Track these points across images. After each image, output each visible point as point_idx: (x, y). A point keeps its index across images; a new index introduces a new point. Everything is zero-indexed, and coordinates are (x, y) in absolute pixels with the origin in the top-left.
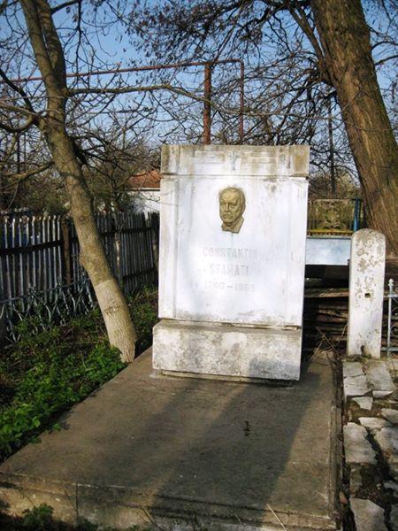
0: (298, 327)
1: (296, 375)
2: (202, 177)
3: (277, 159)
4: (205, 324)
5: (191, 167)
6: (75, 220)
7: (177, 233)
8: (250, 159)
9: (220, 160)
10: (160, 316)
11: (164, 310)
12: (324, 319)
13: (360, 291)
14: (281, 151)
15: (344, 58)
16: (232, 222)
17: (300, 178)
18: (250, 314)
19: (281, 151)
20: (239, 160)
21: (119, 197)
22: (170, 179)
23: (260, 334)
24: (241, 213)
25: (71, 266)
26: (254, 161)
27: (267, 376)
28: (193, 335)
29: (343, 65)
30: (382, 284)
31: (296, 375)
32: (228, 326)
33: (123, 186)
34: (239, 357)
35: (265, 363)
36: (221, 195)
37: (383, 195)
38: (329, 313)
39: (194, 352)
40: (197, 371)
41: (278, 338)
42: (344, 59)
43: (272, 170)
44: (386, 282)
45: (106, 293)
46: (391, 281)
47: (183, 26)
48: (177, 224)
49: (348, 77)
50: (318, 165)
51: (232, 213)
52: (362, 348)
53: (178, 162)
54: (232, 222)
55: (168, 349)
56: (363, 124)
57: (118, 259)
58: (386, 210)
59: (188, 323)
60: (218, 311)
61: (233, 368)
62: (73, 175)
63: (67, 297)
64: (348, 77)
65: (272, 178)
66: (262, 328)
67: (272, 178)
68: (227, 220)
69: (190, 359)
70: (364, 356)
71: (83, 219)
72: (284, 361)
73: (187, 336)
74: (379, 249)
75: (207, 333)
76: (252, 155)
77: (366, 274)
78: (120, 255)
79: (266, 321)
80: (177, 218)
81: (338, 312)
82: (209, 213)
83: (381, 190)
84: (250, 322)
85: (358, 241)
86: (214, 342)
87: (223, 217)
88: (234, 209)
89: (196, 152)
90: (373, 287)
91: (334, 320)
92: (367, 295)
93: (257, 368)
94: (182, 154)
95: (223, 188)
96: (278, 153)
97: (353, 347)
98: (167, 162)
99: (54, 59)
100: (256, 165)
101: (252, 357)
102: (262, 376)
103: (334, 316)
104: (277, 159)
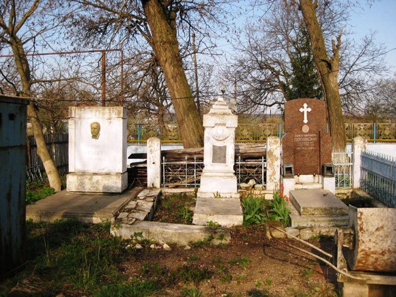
2: (84, 118)
3: (111, 112)
5: (80, 115)
6: (35, 135)
8: (102, 112)
10: (70, 171)
11: (71, 169)
15: (165, 56)
18: (103, 169)
20: (98, 112)
21: (56, 123)
23: (107, 176)
25: (31, 159)
27: (109, 192)
28: (82, 177)
29: (165, 59)
32: (95, 174)
33: (59, 116)
36: (91, 125)
38: (142, 172)
39: (82, 184)
40: (83, 191)
42: (165, 56)
44: (162, 158)
45: (48, 165)
46: (164, 157)
47: (93, 29)
49: (167, 65)
51: (96, 132)
52: (153, 184)
53: (75, 113)
55: (72, 183)
56: (175, 88)
57: (54, 156)
59: (81, 174)
60: (91, 169)
61: (97, 189)
62: (34, 117)
63: (29, 173)
64: (167, 65)
66: (108, 174)
67: (110, 119)
69: (80, 186)
70: (154, 187)
71: (38, 135)
72: (115, 185)
73: (79, 178)
74: (157, 145)
75: (87, 176)
78: (56, 155)
79: (109, 172)
82: (88, 132)
83: (185, 120)
86: (89, 179)
87: (92, 133)
88: (96, 130)
90: (155, 160)
92: (154, 163)
93: (105, 188)
94: (77, 111)
96: (112, 110)
98: (71, 113)
99: (25, 68)
102: (107, 191)
104: (111, 112)
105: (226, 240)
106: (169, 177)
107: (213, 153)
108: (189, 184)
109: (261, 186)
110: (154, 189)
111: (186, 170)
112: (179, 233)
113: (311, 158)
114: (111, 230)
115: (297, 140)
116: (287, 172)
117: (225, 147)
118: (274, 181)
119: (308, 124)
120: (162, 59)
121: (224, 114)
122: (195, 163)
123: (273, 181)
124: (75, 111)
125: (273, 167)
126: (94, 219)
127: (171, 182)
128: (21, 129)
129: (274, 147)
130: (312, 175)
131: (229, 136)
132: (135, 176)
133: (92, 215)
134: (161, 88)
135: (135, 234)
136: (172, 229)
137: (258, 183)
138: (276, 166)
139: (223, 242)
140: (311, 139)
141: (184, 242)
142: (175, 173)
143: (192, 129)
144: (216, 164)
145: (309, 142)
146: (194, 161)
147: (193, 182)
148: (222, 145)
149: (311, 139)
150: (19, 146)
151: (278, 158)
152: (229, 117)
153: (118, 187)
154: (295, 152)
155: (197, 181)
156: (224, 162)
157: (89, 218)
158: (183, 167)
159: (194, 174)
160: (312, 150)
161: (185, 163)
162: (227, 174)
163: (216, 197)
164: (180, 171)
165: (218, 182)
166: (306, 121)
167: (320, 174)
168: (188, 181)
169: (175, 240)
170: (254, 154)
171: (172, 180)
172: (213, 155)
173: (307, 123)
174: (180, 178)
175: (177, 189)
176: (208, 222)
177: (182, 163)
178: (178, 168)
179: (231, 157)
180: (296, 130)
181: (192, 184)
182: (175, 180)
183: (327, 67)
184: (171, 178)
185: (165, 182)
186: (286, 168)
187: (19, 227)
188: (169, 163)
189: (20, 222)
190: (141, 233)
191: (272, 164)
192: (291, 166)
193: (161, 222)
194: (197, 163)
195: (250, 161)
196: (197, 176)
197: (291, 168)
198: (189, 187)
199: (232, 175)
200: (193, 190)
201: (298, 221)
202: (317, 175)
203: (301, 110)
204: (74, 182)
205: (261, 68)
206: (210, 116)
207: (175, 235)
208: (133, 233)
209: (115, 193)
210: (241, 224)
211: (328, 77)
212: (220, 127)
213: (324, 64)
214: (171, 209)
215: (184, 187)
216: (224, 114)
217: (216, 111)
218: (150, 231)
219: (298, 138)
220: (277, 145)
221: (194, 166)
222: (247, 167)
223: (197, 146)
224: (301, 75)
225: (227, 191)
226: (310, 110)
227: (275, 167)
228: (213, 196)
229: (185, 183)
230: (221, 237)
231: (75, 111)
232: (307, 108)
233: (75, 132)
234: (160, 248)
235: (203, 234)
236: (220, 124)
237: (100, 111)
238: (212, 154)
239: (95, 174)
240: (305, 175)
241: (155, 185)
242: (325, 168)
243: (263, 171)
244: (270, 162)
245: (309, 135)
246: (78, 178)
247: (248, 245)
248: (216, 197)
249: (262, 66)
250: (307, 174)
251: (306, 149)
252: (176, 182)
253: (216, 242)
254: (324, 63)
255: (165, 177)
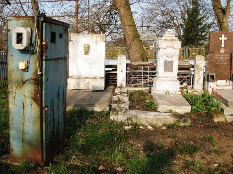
0: (103, 78)
1: (103, 89)
2: (79, 41)
3: (97, 37)
4: (81, 78)
7: (73, 55)
8: (91, 37)
9: (84, 37)
10: (69, 76)
11: (70, 74)
12: (112, 78)
13: (120, 70)
14: (98, 35)
16: (87, 52)
17: (103, 42)
18: (91, 75)
19: (98, 35)
22: (71, 42)
23: (94, 79)
24: (89, 50)
26: (92, 38)
27: (96, 89)
29: (120, 5)
30: (125, 68)
31: (103, 89)
32: (87, 78)
34: (89, 85)
35: (95, 86)
37: (133, 46)
39: (78, 84)
41: (98, 80)
43: (96, 39)
48: (73, 53)
50: (119, 34)
52: (121, 85)
53: (73, 38)
54: (87, 52)
58: (133, 50)
59: (76, 77)
61: (88, 88)
65: (96, 42)
67: (96, 42)
68: (86, 52)
69: (77, 86)
70: (121, 87)
72: (100, 86)
73: (76, 80)
75: (81, 79)
76: (91, 36)
77: (121, 66)
79: (95, 76)
80: (73, 52)
81: (115, 76)
82: (81, 51)
83: (132, 44)
84: (92, 77)
85: (119, 57)
86: (83, 81)
89: (78, 35)
91: (114, 78)
92: (122, 71)
95: (84, 44)
96: (98, 36)
97: (119, 85)
98: (71, 37)
100: (92, 39)
101: (92, 85)
102: (95, 89)
103: (114, 78)
104: (97, 37)
105: (188, 123)
106: (131, 80)
107: (165, 65)
108: (145, 85)
109: (191, 87)
110: (122, 88)
111: (143, 75)
112: (157, 118)
113: (225, 69)
114: (110, 116)
115: (217, 58)
116: (208, 78)
117: (172, 61)
118: (199, 83)
119: (224, 48)
120: (118, 5)
121: (172, 40)
122: (148, 71)
123: (198, 84)
124: (73, 37)
125: (199, 77)
126: (95, 108)
127: (132, 83)
128: (65, 45)
129: (200, 62)
130: (225, 81)
131: (175, 54)
132: (110, 78)
133: (93, 105)
134: (185, 13)
135: (128, 119)
136: (152, 115)
137: (189, 85)
138: (201, 74)
139: (186, 124)
140: (226, 58)
141: (160, 124)
142: (136, 77)
143: (137, 50)
144: (166, 72)
145: (224, 59)
146: (148, 70)
147: (147, 84)
148: (171, 60)
149: (226, 58)
150: (64, 58)
151: (202, 69)
152: (176, 42)
153: (102, 87)
154: (216, 66)
155: (149, 83)
156: (172, 71)
157: (92, 108)
158: (143, 72)
159: (147, 78)
160: (226, 64)
161: (142, 71)
162: (173, 79)
163: (166, 94)
164: (139, 76)
165: (166, 84)
166: (223, 46)
167: (230, 80)
168: (144, 83)
169: (154, 122)
170: (184, 66)
171: (133, 82)
172: (165, 66)
173: (224, 47)
174: (138, 81)
175: (137, 88)
176: (168, 110)
177: (139, 71)
178: (137, 75)
179: (176, 68)
180: (216, 51)
181: (146, 85)
182: (135, 82)
183: (222, 13)
184: (132, 81)
185: (129, 83)
186: (211, 76)
187: (63, 116)
188: (131, 71)
189: (63, 113)
190: (132, 118)
191: (198, 73)
192: (214, 74)
193: (136, 110)
194: (150, 71)
195: (181, 71)
196: (149, 80)
197: (214, 76)
198: (144, 87)
199: (177, 79)
200: (148, 88)
201: (228, 110)
202: (228, 81)
203: (220, 39)
204: (73, 83)
205: (163, 15)
206: (163, 41)
207: (154, 120)
208: (126, 118)
209: (100, 90)
210: (190, 112)
211: (223, 19)
212: (169, 48)
213: (220, 11)
214: (143, 102)
215: (141, 86)
216: (172, 40)
217: (167, 38)
218: (138, 116)
219: (217, 57)
220: (202, 61)
221: (148, 73)
222: (182, 75)
223: (140, 60)
224: (192, 18)
225: (173, 90)
226: (226, 39)
227: (200, 75)
228: (164, 93)
229: (142, 83)
230: (185, 121)
231: (73, 36)
232: (224, 37)
233: (73, 50)
234: (146, 128)
235: (173, 119)
236: (170, 47)
237: (89, 37)
238: (164, 65)
239: (87, 78)
240: (221, 81)
241: (123, 85)
242: (210, 76)
243: (192, 77)
244: (197, 72)
245: (224, 55)
246: (75, 81)
247: (204, 126)
248: (166, 94)
249: (164, 14)
250: (222, 80)
251: (222, 63)
252: (135, 83)
253: (182, 124)
254: (220, 10)
255: (129, 80)
